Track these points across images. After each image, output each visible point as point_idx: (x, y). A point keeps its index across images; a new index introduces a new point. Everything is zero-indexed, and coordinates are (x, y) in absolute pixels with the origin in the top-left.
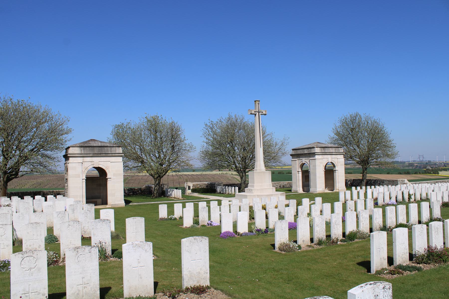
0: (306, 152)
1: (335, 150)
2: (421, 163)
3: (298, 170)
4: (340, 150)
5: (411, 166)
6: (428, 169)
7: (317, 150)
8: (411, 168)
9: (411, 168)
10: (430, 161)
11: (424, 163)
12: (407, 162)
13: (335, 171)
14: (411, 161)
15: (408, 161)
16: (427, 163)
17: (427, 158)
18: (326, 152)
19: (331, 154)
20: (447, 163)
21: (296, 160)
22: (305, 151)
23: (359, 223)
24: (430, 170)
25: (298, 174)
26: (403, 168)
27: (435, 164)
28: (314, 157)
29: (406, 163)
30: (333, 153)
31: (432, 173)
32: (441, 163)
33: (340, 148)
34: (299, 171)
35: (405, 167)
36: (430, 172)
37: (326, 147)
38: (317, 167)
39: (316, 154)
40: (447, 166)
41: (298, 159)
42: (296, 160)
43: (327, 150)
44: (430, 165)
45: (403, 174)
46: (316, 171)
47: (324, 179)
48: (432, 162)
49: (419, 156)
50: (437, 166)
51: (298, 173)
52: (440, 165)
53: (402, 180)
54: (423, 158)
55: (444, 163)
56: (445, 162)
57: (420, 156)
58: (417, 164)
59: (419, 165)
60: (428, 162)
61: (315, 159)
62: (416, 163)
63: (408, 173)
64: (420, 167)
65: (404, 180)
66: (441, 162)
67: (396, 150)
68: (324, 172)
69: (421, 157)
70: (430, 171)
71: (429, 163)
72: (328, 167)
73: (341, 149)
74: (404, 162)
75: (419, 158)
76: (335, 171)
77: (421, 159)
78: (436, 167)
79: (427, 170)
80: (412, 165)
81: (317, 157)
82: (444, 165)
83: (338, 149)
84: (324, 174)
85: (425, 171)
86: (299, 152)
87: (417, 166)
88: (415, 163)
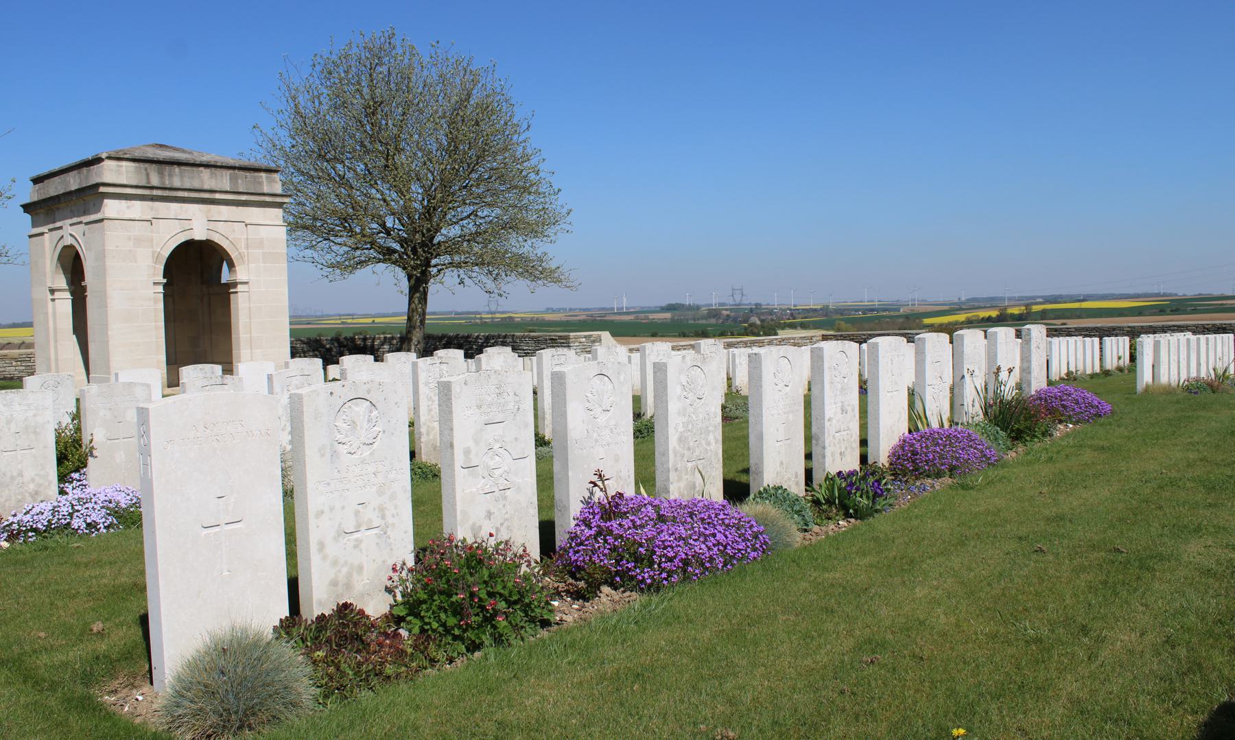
0: (73, 182)
1: (233, 179)
2: (736, 309)
3: (53, 282)
4: (261, 183)
5: (714, 317)
6: (752, 323)
7: (111, 172)
8: (713, 321)
9: (713, 321)
10: (760, 305)
11: (743, 309)
12: (704, 306)
13: (235, 284)
14: (716, 304)
15: (707, 305)
16: (751, 310)
17: (750, 300)
18: (177, 183)
19: (206, 198)
20: (798, 310)
21: (42, 234)
22: (72, 181)
23: (763, 396)
24: (758, 325)
25: (50, 303)
26: (695, 320)
27: (771, 312)
28: (98, 210)
29: (703, 308)
30: (218, 196)
31: (761, 333)
32: (785, 310)
33: (263, 175)
34: (55, 286)
35: (698, 319)
36: (756, 331)
37: (180, 164)
38: (109, 263)
39: (102, 189)
40: (797, 316)
41: (51, 226)
42: (42, 234)
43: (177, 178)
44: (758, 315)
45: (692, 337)
46: (105, 283)
47: (162, 324)
48: (763, 307)
49: (733, 290)
50: (774, 317)
51: (53, 300)
52: (781, 314)
53: (591, 336)
54: (743, 295)
55: (790, 310)
56: (793, 308)
57: (736, 290)
58: (728, 312)
59: (733, 314)
60: (754, 307)
61: (101, 220)
62: (727, 310)
63: (703, 333)
64: (735, 320)
65: (600, 336)
66: (783, 307)
67: (559, 203)
68: (160, 289)
69: (737, 292)
70: (757, 328)
71: (756, 308)
72: (502, 318)
73: (271, 181)
74: (698, 308)
75: (733, 296)
76: (235, 284)
77: (738, 298)
78: (772, 320)
79: (752, 325)
80: (717, 315)
81: (111, 207)
82: (792, 315)
83: (255, 178)
84: (156, 301)
85: (746, 328)
86: (54, 188)
87: (728, 316)
88: (723, 309)
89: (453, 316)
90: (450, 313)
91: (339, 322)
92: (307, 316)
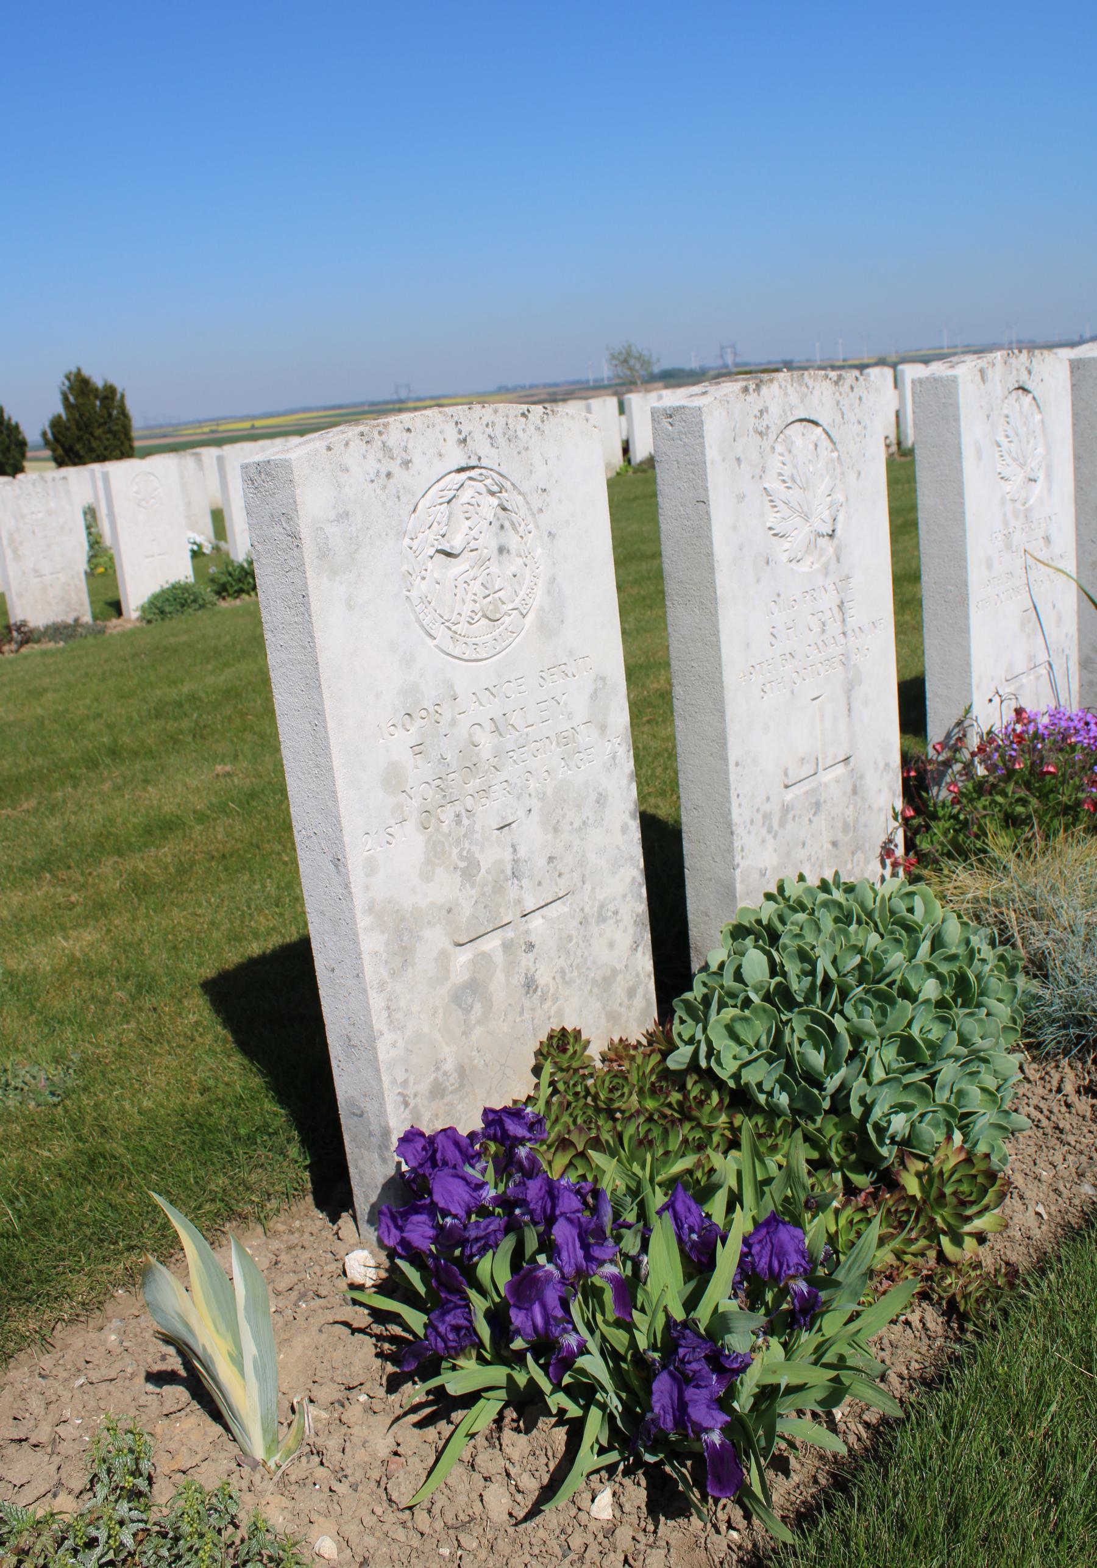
89: (366, 408)
90: (362, 404)
91: (206, 430)
92: (161, 426)
